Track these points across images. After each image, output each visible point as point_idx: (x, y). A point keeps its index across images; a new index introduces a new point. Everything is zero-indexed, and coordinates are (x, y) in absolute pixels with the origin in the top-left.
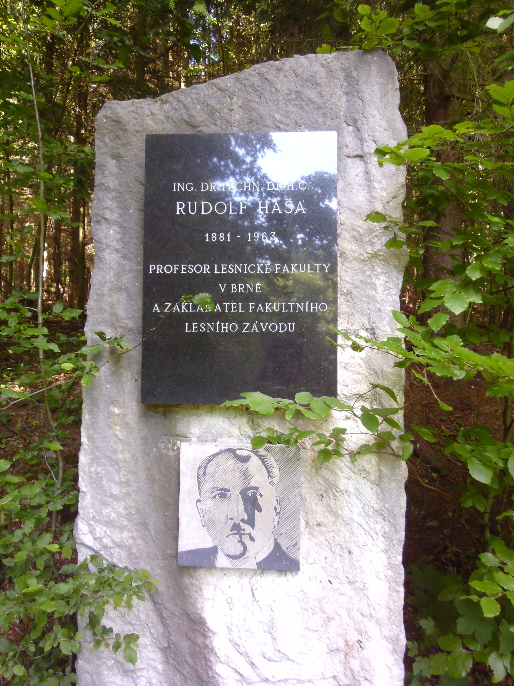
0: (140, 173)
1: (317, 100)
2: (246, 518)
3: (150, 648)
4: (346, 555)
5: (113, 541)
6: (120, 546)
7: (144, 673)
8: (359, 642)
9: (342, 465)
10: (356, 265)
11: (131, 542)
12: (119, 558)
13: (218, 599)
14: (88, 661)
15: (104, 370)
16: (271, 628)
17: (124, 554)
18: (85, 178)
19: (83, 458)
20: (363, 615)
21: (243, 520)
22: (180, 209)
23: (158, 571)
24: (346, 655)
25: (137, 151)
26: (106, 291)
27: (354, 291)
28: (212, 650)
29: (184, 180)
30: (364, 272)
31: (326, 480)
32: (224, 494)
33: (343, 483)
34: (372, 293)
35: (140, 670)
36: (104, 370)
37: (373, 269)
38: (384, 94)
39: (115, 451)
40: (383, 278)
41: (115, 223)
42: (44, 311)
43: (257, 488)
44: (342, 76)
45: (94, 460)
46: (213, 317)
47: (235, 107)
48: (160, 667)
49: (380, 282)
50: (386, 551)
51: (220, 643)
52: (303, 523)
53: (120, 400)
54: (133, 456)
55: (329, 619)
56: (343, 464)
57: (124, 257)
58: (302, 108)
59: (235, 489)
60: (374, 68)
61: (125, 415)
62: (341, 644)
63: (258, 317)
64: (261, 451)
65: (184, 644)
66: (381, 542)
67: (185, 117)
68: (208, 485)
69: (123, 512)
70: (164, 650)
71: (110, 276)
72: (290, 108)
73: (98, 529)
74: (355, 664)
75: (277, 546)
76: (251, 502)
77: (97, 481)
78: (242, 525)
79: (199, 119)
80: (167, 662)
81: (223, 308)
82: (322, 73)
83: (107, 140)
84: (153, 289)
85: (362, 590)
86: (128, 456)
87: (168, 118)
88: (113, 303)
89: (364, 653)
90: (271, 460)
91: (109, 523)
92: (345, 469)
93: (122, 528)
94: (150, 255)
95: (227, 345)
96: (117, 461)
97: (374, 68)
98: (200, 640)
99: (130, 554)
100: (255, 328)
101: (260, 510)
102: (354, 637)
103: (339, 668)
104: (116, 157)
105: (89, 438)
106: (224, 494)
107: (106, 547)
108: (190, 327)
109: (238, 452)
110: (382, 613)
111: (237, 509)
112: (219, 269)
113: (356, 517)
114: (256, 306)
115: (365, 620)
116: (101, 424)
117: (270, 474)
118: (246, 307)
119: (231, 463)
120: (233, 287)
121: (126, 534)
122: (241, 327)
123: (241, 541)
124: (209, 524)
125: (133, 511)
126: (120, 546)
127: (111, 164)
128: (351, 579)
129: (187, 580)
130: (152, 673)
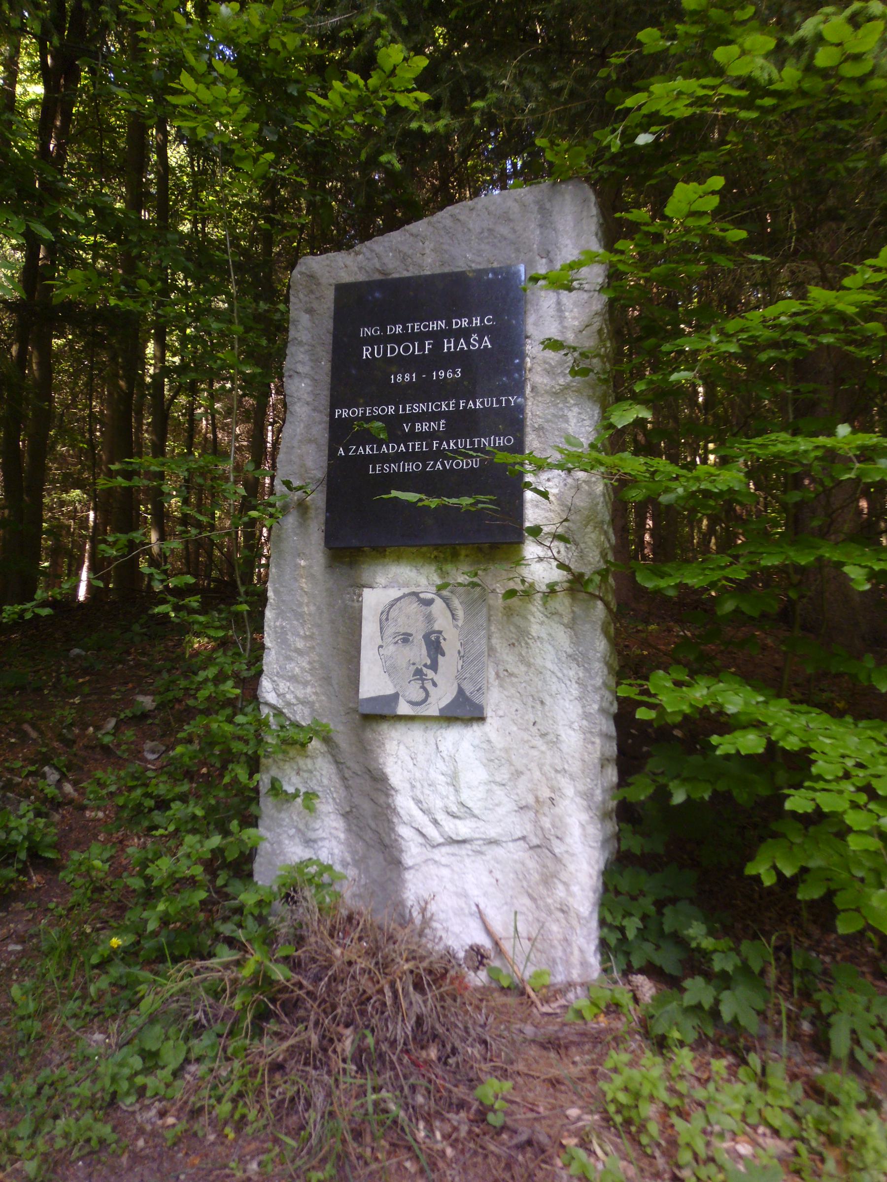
0: (329, 324)
1: (511, 236)
2: (429, 662)
3: (332, 816)
4: (539, 706)
5: (296, 698)
6: (303, 702)
7: (326, 843)
8: (552, 799)
9: (534, 609)
10: (548, 399)
11: (314, 698)
12: (302, 716)
13: (404, 757)
14: (268, 829)
15: (291, 521)
16: (454, 780)
17: (307, 711)
18: (276, 329)
19: (269, 614)
20: (556, 771)
21: (425, 665)
22: (366, 354)
23: (341, 728)
24: (537, 812)
25: (327, 304)
26: (295, 444)
27: (546, 425)
28: (394, 811)
29: (370, 325)
30: (556, 405)
31: (518, 627)
32: (406, 639)
33: (535, 629)
34: (564, 425)
35: (322, 839)
36: (291, 521)
37: (565, 401)
38: (578, 221)
39: (300, 605)
40: (576, 409)
41: (306, 375)
42: (275, 1004)
43: (440, 632)
44: (536, 208)
45: (280, 614)
46: (398, 457)
47: (427, 251)
48: (342, 836)
49: (572, 414)
50: (580, 699)
51: (403, 802)
52: (492, 674)
53: (307, 551)
54: (318, 608)
55: (518, 773)
56: (536, 608)
57: (314, 410)
58: (494, 245)
59: (418, 631)
60: (568, 197)
61: (311, 567)
62: (531, 800)
63: (441, 454)
64: (445, 593)
65: (366, 806)
66: (575, 690)
67: (378, 266)
68: (390, 630)
69: (307, 666)
70: (346, 815)
71: (300, 429)
72: (483, 246)
73: (282, 685)
74: (546, 822)
75: (461, 691)
76: (435, 647)
77: (282, 640)
78: (425, 670)
79: (391, 266)
80: (349, 830)
81: (407, 447)
82: (516, 208)
83: (301, 296)
84: (339, 432)
85: (554, 743)
86: (313, 608)
87: (360, 268)
88: (301, 447)
89: (557, 810)
90: (456, 603)
91: (293, 679)
92: (538, 614)
93: (305, 684)
94: (336, 402)
95: (423, 500)
96: (302, 615)
97: (568, 197)
98: (382, 800)
99: (313, 710)
100: (439, 466)
101: (443, 654)
102: (545, 793)
103: (529, 827)
104: (310, 311)
105: (276, 592)
106: (406, 639)
107: (289, 704)
108: (374, 469)
109: (422, 596)
110: (575, 767)
111: (419, 653)
112: (404, 409)
113: (549, 665)
114: (441, 444)
115: (559, 776)
116: (287, 577)
117: (454, 616)
118: (429, 446)
119: (414, 607)
120: (418, 426)
121: (309, 690)
122: (425, 466)
123: (423, 687)
124: (391, 670)
125: (317, 665)
126: (303, 702)
127: (305, 318)
128: (543, 731)
129: (369, 735)
130: (334, 843)
